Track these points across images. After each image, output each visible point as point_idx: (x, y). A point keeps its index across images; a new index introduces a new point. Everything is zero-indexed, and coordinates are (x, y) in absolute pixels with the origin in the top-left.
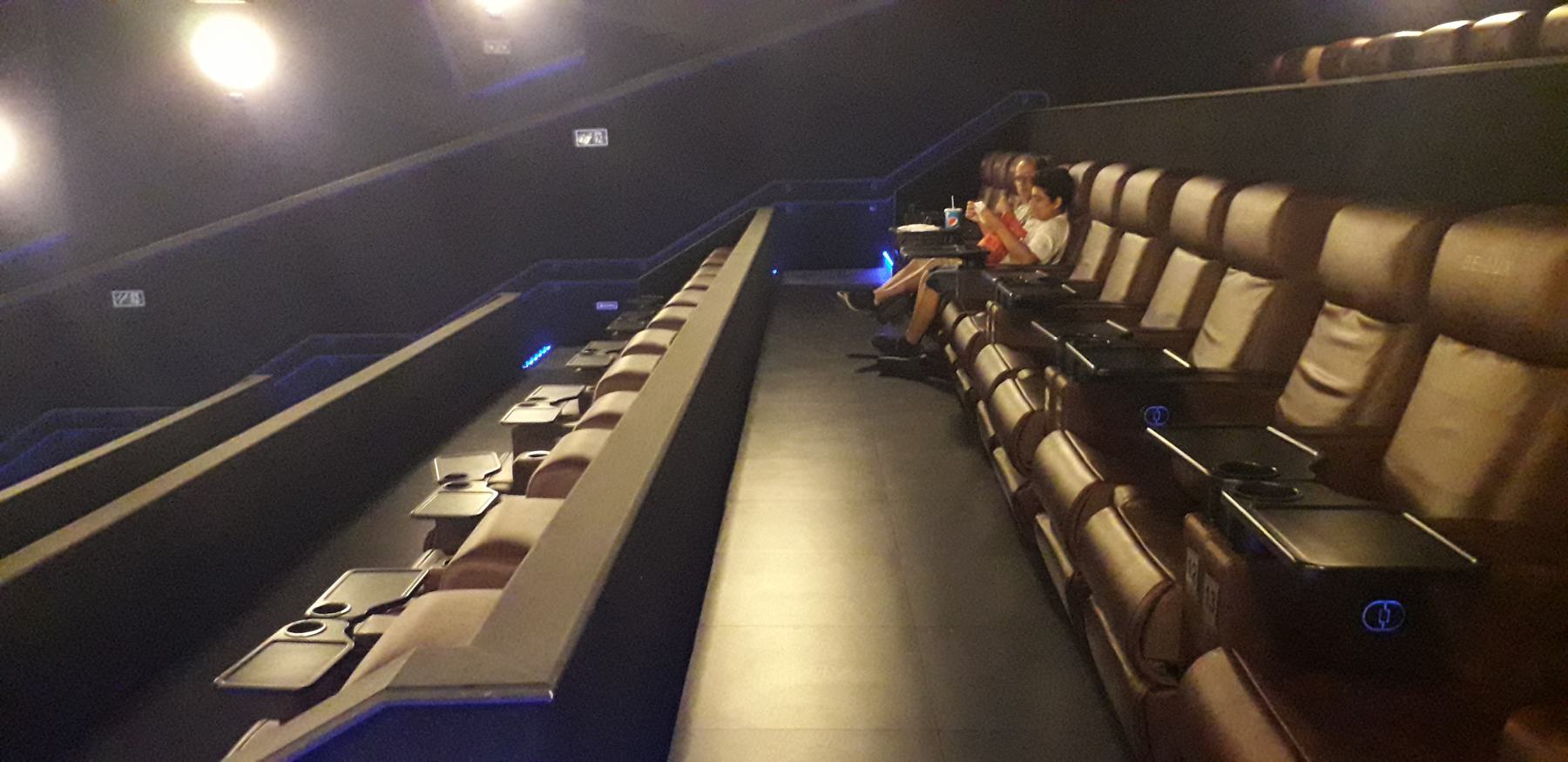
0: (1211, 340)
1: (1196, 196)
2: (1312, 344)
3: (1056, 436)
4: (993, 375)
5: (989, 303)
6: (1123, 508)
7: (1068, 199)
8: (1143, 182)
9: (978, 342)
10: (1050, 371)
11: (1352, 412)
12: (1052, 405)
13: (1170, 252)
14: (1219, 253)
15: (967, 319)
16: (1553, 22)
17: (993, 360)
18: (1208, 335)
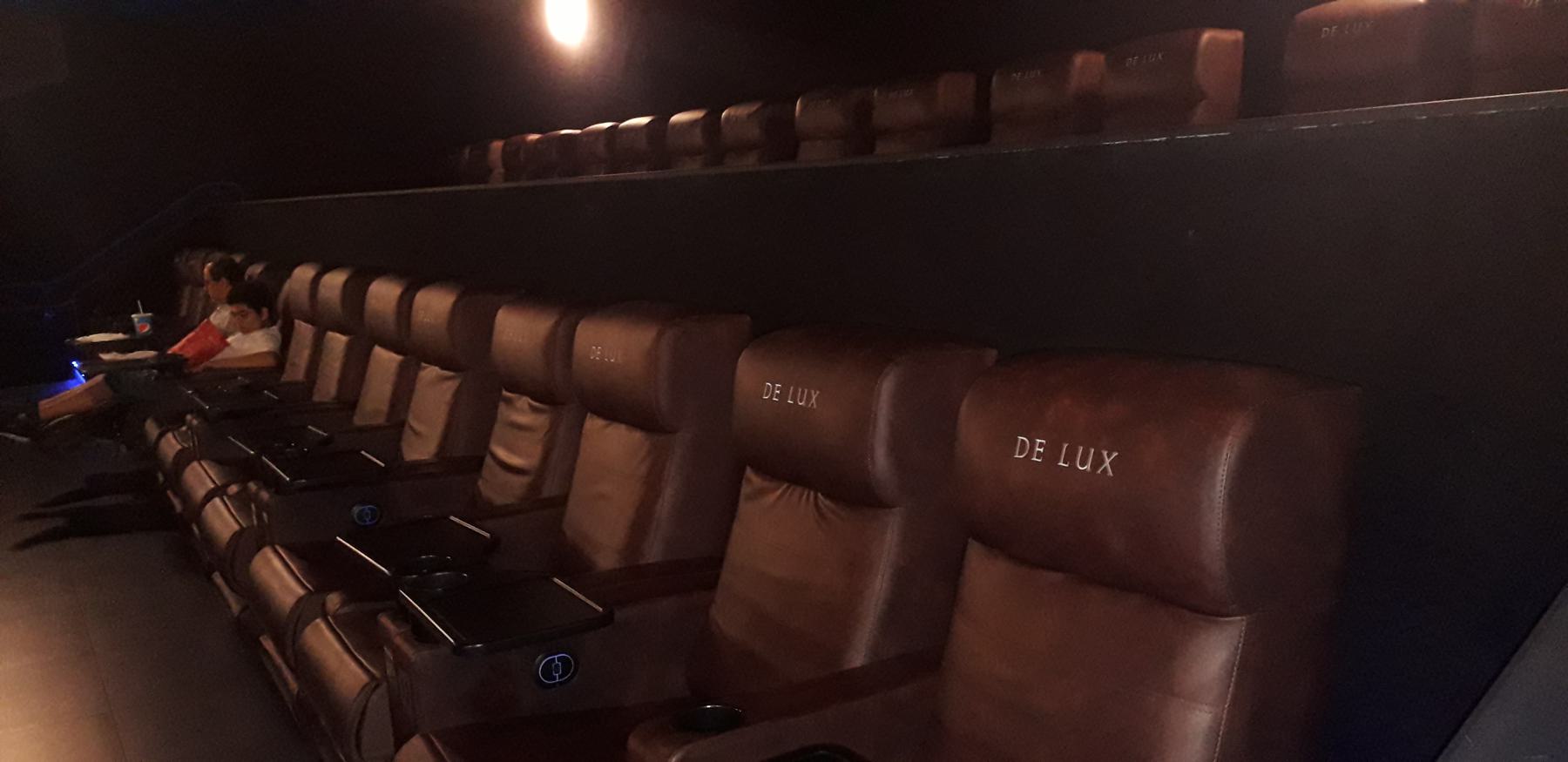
0: (417, 434)
1: (384, 293)
2: (497, 428)
3: (268, 551)
4: (201, 493)
5: (189, 417)
6: (334, 617)
7: (259, 301)
8: (335, 280)
9: (183, 459)
10: (252, 486)
11: (535, 488)
12: (259, 517)
13: (371, 349)
14: (414, 352)
15: (170, 435)
16: (675, 125)
17: (201, 477)
18: (411, 428)
